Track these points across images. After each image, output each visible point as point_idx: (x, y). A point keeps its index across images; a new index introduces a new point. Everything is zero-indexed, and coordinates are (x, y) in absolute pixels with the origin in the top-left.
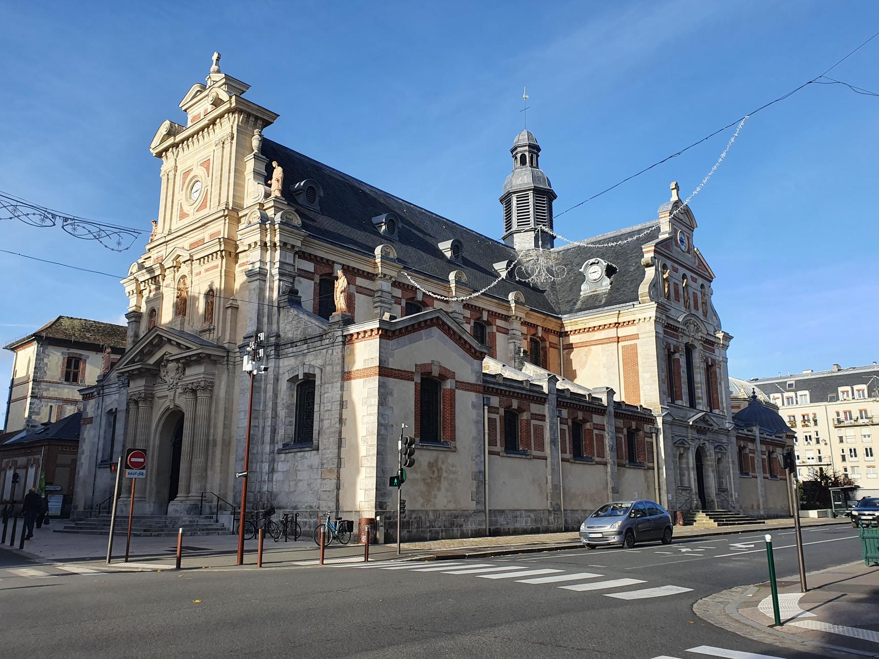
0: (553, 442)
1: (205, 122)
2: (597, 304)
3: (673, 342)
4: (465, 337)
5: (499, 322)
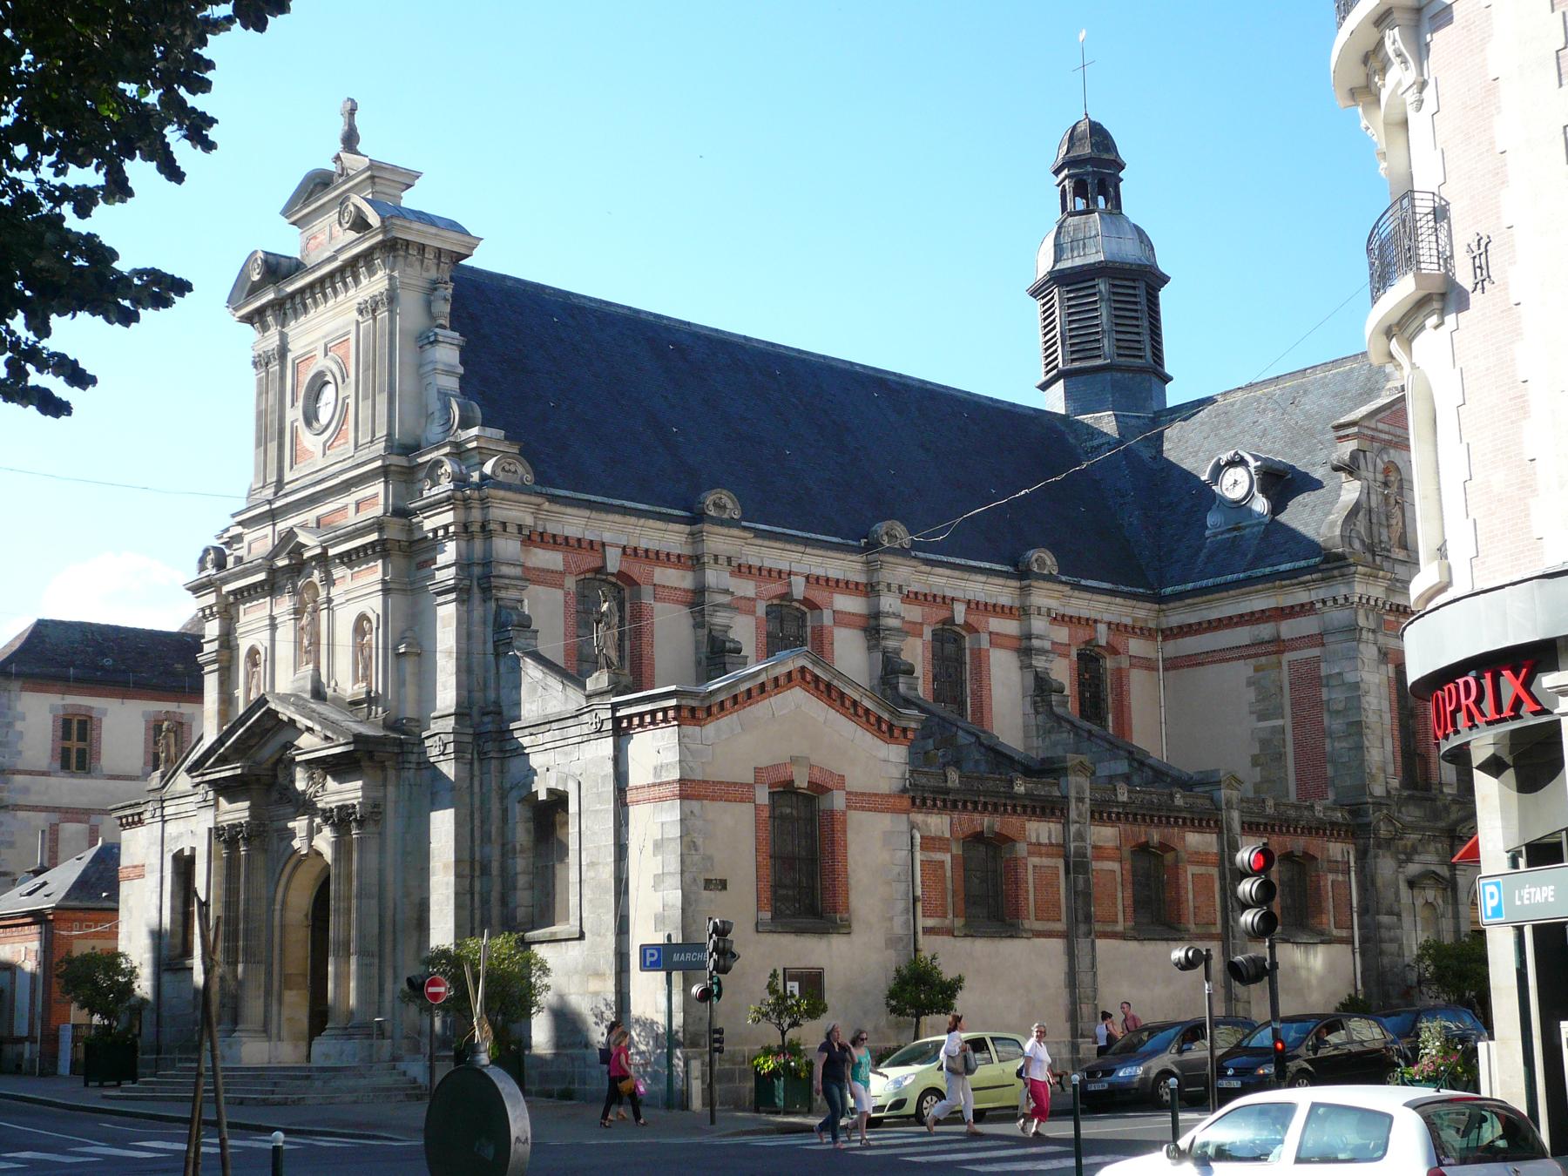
5: (997, 624)
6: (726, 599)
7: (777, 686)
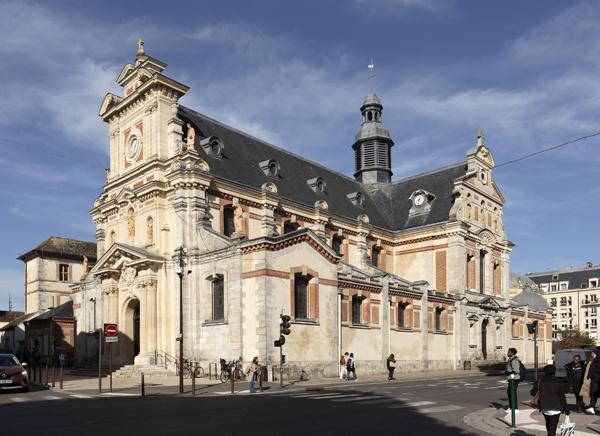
0: (385, 317)
1: (136, 95)
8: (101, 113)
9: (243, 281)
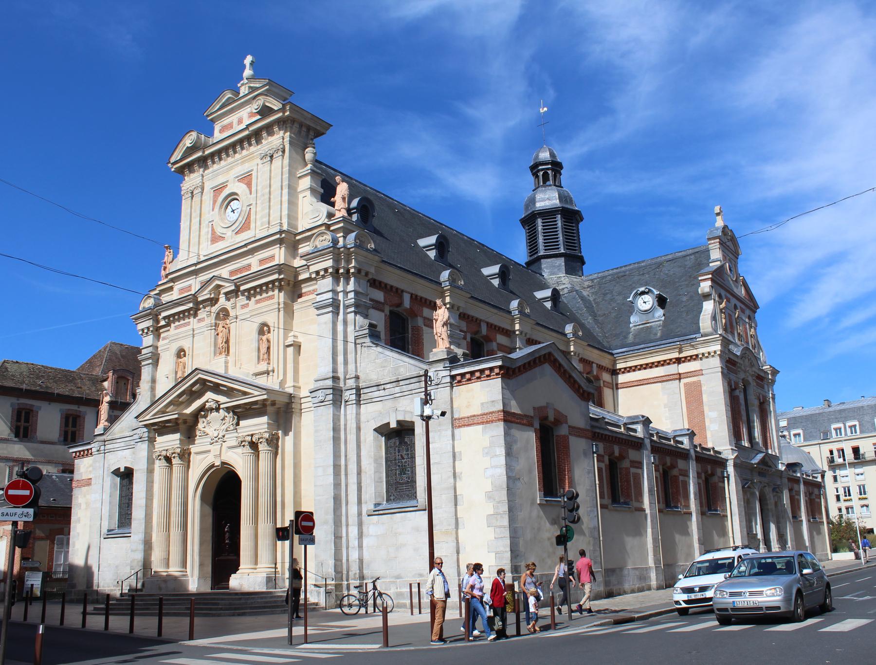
1: (246, 133)
2: (652, 337)
3: (733, 377)
4: (574, 375)
6: (732, 246)
7: (540, 361)
8: (173, 160)
9: (457, 431)
